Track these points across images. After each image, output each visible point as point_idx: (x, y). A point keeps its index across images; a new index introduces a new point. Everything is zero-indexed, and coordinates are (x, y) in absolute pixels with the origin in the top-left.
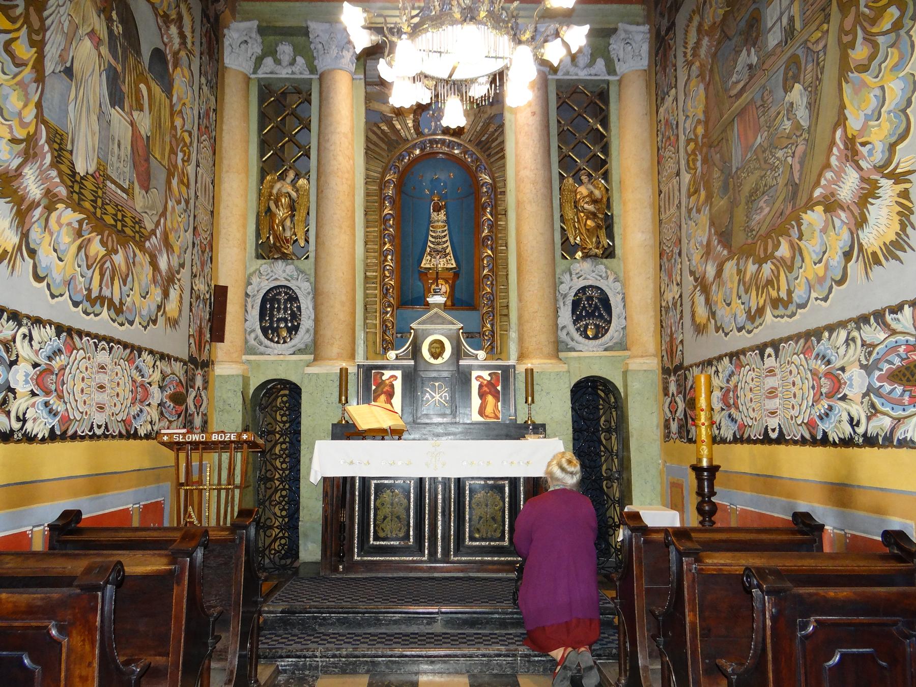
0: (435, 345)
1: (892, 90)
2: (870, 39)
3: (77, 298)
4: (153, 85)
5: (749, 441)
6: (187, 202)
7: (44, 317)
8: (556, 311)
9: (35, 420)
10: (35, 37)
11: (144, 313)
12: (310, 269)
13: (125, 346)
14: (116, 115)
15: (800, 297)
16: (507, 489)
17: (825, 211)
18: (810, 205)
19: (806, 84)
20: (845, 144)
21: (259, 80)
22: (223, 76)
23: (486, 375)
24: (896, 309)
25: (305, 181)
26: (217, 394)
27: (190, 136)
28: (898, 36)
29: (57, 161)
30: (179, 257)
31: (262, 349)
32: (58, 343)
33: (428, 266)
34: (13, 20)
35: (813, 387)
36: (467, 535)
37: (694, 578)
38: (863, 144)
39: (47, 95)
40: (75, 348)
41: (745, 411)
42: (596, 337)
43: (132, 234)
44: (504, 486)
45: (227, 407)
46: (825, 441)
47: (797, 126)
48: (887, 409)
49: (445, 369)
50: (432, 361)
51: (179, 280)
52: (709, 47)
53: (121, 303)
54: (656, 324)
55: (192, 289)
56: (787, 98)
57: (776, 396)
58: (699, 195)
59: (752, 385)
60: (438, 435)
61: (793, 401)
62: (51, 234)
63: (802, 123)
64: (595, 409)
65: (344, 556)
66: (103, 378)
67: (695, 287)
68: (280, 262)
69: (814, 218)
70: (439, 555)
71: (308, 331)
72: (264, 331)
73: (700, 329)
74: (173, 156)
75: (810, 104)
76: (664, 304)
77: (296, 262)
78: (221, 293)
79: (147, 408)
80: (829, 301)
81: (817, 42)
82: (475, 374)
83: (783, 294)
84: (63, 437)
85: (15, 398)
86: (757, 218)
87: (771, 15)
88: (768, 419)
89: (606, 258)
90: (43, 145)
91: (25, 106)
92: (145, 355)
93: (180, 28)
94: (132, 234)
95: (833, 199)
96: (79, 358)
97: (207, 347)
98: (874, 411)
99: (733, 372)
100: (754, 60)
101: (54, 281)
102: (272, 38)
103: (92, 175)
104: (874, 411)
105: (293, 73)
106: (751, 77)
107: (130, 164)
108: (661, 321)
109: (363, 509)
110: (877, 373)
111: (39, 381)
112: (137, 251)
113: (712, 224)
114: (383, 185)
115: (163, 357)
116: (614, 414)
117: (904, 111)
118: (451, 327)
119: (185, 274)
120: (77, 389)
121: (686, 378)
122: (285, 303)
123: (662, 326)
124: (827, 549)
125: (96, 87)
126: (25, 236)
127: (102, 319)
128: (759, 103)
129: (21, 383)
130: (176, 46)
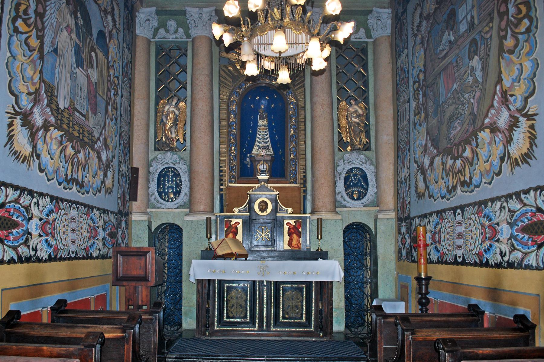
0: (262, 204)
1: (526, 66)
2: (515, 35)
3: (60, 181)
4: (98, 52)
5: (446, 263)
6: (116, 119)
7: (45, 192)
8: (335, 183)
9: (41, 250)
10: (40, 34)
11: (94, 186)
12: (187, 157)
13: (85, 206)
14: (79, 72)
15: (476, 181)
16: (304, 290)
17: (491, 132)
18: (482, 128)
19: (481, 57)
20: (502, 95)
21: (156, 42)
22: (135, 41)
23: (292, 222)
24: (527, 192)
25: (184, 104)
26: (133, 231)
27: (118, 80)
28: (529, 36)
29: (50, 103)
30: (112, 152)
31: (159, 205)
32: (51, 206)
33: (257, 153)
34: (29, 26)
35: (482, 234)
36: (281, 316)
37: (410, 343)
38: (512, 96)
39: (45, 66)
40: (60, 209)
41: (444, 245)
42: (358, 199)
43: (88, 141)
44: (303, 288)
45: (139, 240)
46: (487, 264)
47: (476, 81)
48: (520, 248)
49: (268, 218)
50: (260, 213)
51: (112, 166)
52: (427, 27)
53: (83, 182)
54: (394, 191)
55: (119, 170)
56: (470, 64)
57: (462, 238)
58: (421, 115)
59: (448, 230)
60: (263, 258)
61: (471, 241)
62: (47, 145)
63: (479, 79)
64: (358, 239)
65: (209, 327)
66: (74, 225)
67: (418, 171)
68: (169, 153)
69: (485, 135)
70: (265, 327)
71: (186, 194)
72: (160, 194)
73: (420, 196)
74: (109, 93)
75: (483, 69)
76: (399, 179)
77: (178, 153)
78: (135, 171)
79: (97, 241)
80: (492, 185)
81: (486, 33)
82: (286, 221)
83: (467, 179)
84: (55, 259)
85: (32, 238)
86: (454, 132)
87: (461, 13)
88: (457, 251)
89: (365, 150)
90: (43, 95)
91: (34, 73)
92: (95, 211)
93: (113, 16)
94: (88, 141)
95: (495, 126)
96: (62, 215)
97: (128, 204)
98: (513, 249)
99: (438, 222)
100: (452, 38)
101: (49, 171)
102: (164, 17)
103: (67, 109)
104: (513, 249)
105: (176, 38)
106: (451, 48)
107: (86, 100)
108: (398, 190)
109: (220, 299)
110: (516, 227)
111: (43, 228)
112: (90, 151)
113: (428, 133)
114: (229, 103)
115: (105, 211)
116: (369, 244)
117: (532, 79)
118: (272, 193)
119: (115, 162)
120: (61, 232)
121: (411, 225)
122: (172, 177)
123: (398, 193)
124: (486, 325)
125: (70, 57)
126: (34, 147)
127: (73, 192)
128: (455, 64)
129: (34, 230)
130: (111, 27)
